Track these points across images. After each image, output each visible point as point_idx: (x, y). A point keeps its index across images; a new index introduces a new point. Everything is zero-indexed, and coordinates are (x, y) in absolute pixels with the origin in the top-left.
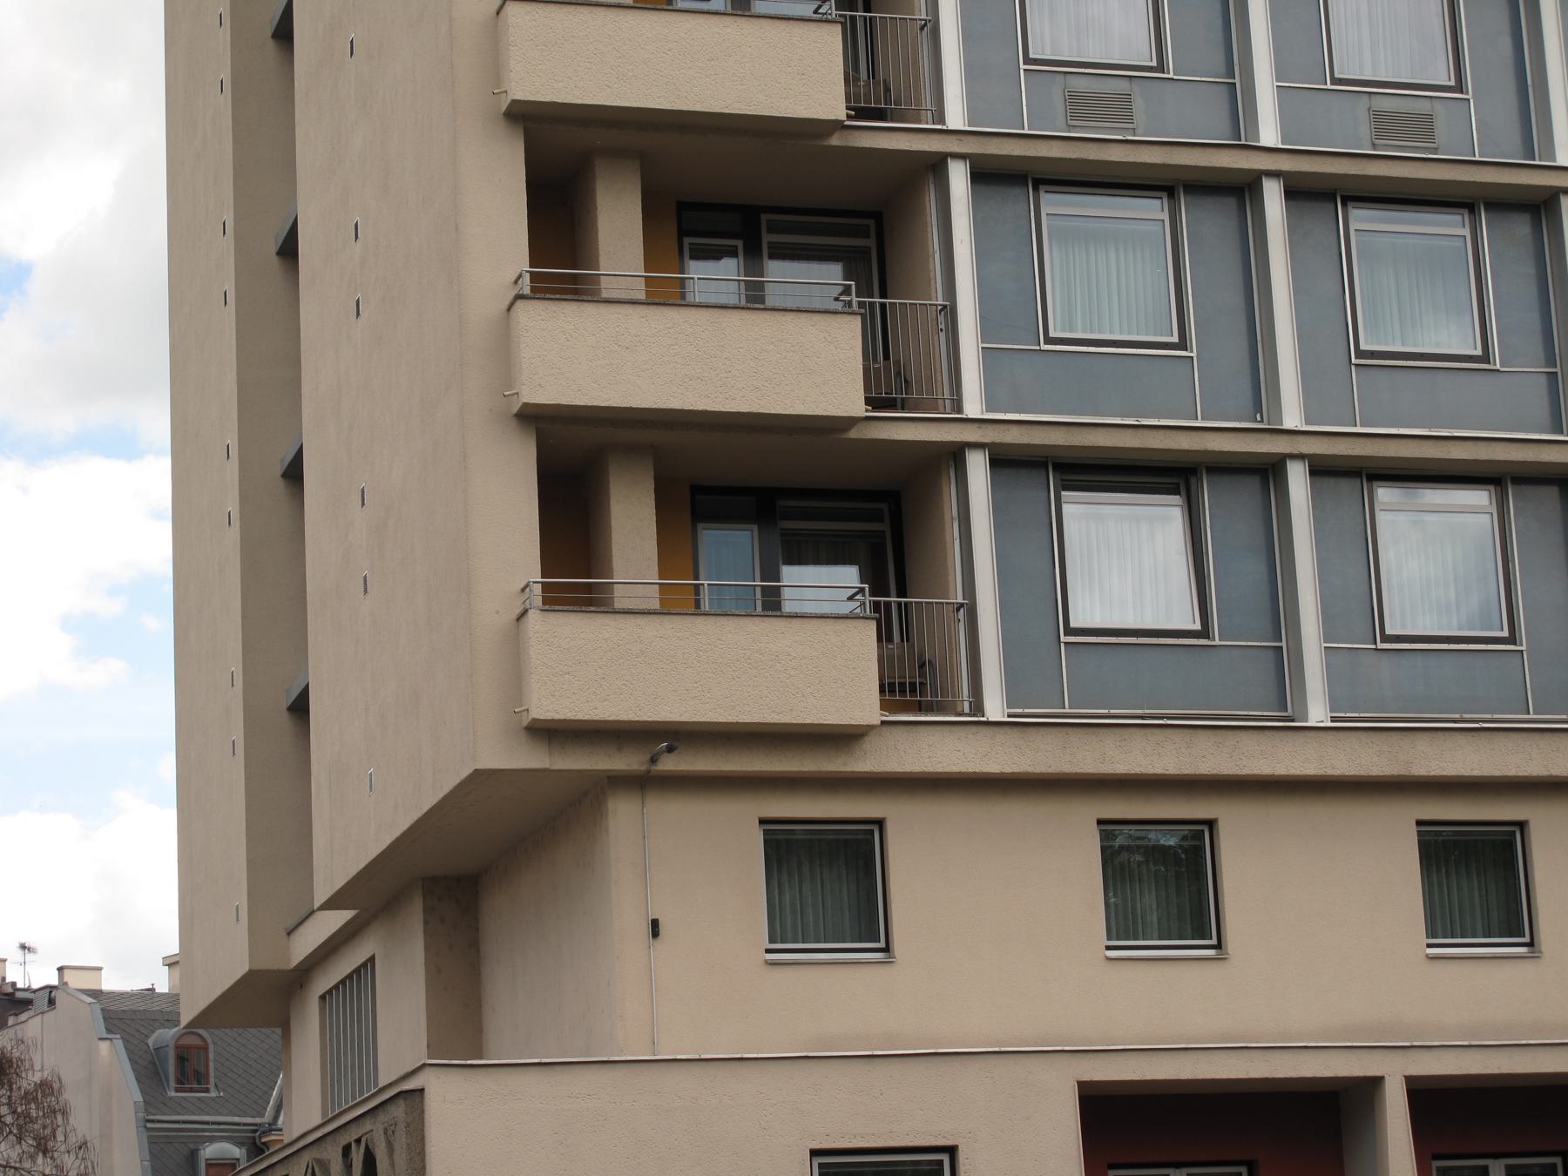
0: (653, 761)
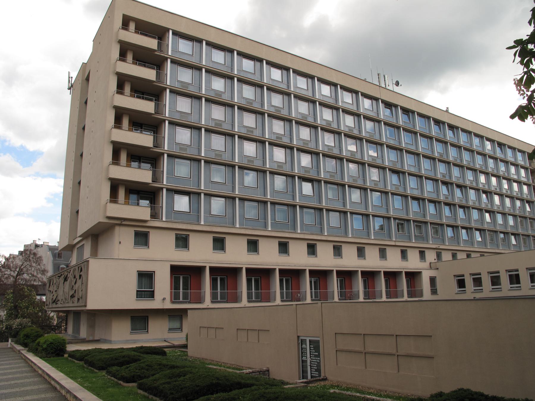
0: (122, 222)
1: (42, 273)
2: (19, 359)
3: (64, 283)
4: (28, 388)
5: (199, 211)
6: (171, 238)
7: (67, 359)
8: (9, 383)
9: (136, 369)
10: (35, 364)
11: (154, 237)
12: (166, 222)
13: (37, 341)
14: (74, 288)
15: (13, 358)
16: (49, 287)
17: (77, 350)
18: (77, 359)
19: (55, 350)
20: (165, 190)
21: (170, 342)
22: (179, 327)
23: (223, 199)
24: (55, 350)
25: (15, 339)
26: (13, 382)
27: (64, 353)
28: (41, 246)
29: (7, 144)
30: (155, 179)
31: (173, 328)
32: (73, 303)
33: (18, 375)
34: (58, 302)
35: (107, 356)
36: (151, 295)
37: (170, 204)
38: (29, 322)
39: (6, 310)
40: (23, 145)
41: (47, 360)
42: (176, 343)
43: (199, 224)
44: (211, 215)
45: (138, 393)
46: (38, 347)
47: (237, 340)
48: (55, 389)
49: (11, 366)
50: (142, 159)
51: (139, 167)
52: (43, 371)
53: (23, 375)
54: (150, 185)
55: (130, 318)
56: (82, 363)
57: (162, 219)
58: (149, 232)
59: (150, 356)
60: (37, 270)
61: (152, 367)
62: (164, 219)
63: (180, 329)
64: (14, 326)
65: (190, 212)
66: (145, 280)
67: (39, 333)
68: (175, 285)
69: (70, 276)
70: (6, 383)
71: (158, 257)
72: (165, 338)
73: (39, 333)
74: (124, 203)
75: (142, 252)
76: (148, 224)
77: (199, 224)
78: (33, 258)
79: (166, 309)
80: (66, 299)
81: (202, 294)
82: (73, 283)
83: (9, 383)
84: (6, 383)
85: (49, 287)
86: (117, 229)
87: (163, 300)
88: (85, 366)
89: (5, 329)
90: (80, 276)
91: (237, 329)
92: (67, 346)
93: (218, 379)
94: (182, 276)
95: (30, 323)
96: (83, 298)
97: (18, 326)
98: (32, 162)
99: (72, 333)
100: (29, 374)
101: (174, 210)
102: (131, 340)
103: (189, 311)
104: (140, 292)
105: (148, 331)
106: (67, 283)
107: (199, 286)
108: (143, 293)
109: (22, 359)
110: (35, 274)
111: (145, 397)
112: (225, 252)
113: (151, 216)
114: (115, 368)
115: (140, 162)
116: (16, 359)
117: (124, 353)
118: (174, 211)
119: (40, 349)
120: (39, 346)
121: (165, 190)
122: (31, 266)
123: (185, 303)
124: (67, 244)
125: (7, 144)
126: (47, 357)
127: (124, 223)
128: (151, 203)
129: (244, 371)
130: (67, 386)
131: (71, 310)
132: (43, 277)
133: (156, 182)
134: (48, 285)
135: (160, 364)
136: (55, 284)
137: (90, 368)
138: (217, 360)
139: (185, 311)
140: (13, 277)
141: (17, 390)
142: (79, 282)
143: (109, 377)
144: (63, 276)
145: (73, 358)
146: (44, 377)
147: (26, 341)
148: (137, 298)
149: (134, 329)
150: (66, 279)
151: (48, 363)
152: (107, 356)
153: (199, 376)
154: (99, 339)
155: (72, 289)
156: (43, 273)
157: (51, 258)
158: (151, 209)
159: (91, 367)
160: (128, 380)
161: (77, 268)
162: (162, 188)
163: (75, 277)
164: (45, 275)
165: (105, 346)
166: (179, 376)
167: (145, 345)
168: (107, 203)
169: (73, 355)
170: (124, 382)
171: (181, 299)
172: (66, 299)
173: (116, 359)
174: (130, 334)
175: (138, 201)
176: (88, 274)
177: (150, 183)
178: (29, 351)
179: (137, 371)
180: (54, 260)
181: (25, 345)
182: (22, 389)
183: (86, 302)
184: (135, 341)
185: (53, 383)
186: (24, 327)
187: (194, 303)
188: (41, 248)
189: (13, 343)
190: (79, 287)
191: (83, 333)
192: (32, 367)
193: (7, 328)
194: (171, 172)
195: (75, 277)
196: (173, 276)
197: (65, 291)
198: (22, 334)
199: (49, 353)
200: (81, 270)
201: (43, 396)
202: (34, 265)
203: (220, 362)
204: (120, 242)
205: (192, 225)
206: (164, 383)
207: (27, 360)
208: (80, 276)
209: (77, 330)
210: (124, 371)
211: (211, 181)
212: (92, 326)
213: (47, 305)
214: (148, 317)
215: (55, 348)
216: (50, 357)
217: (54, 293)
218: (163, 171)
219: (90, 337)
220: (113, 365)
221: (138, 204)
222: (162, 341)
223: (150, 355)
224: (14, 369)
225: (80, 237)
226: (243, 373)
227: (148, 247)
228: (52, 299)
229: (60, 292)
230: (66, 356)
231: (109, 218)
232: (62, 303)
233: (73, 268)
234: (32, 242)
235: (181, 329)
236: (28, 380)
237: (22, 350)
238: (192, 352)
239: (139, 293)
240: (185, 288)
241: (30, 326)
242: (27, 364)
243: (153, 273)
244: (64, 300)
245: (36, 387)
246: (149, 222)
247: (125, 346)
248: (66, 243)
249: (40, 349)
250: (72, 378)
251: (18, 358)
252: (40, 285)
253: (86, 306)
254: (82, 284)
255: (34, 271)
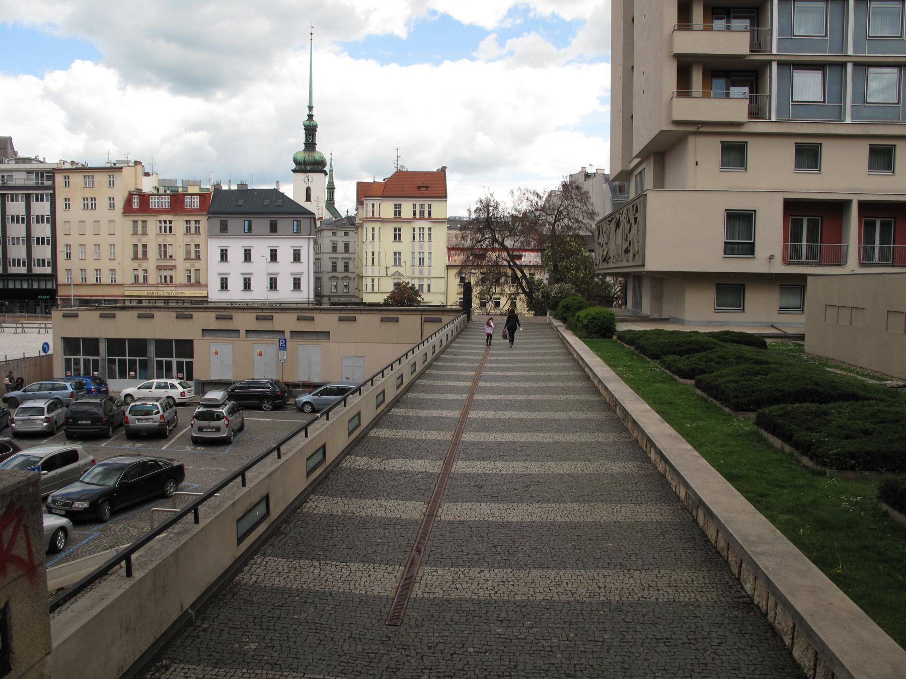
0: (698, 129)
1: (590, 216)
2: (555, 338)
3: (616, 231)
4: (556, 373)
5: (842, 97)
6: (787, 152)
7: (616, 342)
8: (534, 365)
9: (701, 361)
10: (571, 345)
11: (755, 152)
12: (778, 123)
13: (577, 314)
14: (628, 239)
15: (547, 336)
16: (598, 238)
17: (630, 331)
18: (627, 343)
19: (599, 328)
20: (774, 66)
21: (780, 328)
22: (799, 306)
23: (895, 70)
24: (599, 328)
25: (553, 312)
26: (539, 365)
27: (613, 334)
28: (593, 175)
29: (531, 15)
30: (757, 45)
31: (788, 306)
32: (628, 261)
33: (548, 357)
34: (609, 261)
35: (666, 340)
36: (749, 250)
37: (786, 87)
38: (572, 288)
39: (548, 272)
40: (556, 12)
41: (589, 341)
42: (790, 331)
43: (841, 123)
44: (867, 103)
45: (694, 394)
46: (578, 323)
47: (887, 330)
48: (588, 377)
49: (542, 346)
50: (733, 13)
51: (728, 29)
52: (578, 354)
53: (554, 358)
54: (747, 58)
55: (714, 286)
56: (632, 348)
57: (770, 118)
58: (747, 143)
59: (733, 346)
60: (582, 212)
61: (726, 359)
62: (774, 118)
63: (800, 308)
64: (553, 294)
65: (824, 102)
66: (739, 225)
67: (582, 304)
68: (792, 233)
69: (623, 220)
70: (531, 365)
71: (763, 185)
72: (772, 323)
73: (582, 304)
74: (701, 96)
75: (734, 178)
76: (745, 129)
77: (841, 123)
78: (576, 195)
79: (777, 274)
80: (618, 255)
81: (844, 250)
82: (627, 231)
83: (534, 365)
84: (531, 365)
85: (598, 238)
86: (691, 140)
87: (770, 258)
88: (636, 352)
89: (542, 298)
90: (636, 219)
91: (888, 311)
92: (617, 324)
93: (817, 384)
94: (807, 218)
95: (574, 290)
96: (640, 254)
97: (557, 293)
98: (570, 39)
99: (632, 308)
100: (562, 358)
101: (794, 100)
102: (716, 322)
103: (809, 278)
104: (731, 246)
105: (743, 309)
106: (620, 231)
107: (839, 235)
108: (737, 246)
109: (559, 338)
110: (580, 218)
111: (702, 398)
112: (893, 172)
113: (749, 114)
114: (671, 357)
115: (730, 18)
116: (551, 338)
117: (693, 338)
118: (792, 101)
119: (580, 325)
120: (579, 321)
121: (774, 66)
122: (574, 207)
123: (811, 264)
124: (620, 170)
125: (531, 15)
126: (588, 337)
127: (702, 129)
128: (751, 91)
129: (889, 382)
130: (599, 374)
131: (631, 272)
132: (591, 222)
133: (760, 52)
134: (596, 234)
135: (740, 356)
136: (605, 232)
137: (641, 355)
138: (851, 362)
139: (804, 277)
140: (550, 223)
141: (542, 374)
142: (634, 228)
143: (663, 369)
144: (614, 221)
145: (622, 341)
146: (579, 363)
147: (565, 315)
148: (725, 254)
149: (721, 304)
150: (618, 225)
151: (587, 345)
152: (666, 340)
153: (788, 377)
154: (667, 317)
155: (626, 240)
156: (592, 217)
157: (609, 194)
158: (751, 102)
159: (643, 354)
160: (685, 375)
161: (631, 207)
162: (769, 63)
163: (629, 222)
164: (594, 220)
165: (669, 328)
166: (756, 374)
167: (732, 329)
168: (672, 98)
169: (622, 337)
170: (679, 376)
171: (804, 259)
172: (618, 255)
173: (678, 345)
174: (715, 312)
175: (728, 89)
176: (645, 217)
177: (746, 56)
178: (568, 328)
179: (700, 363)
180: (613, 197)
181: (564, 320)
182: (548, 373)
183: (644, 260)
184: (723, 323)
185: (587, 369)
186: (566, 296)
187: (826, 265)
188: (594, 179)
189: (551, 318)
190: (634, 236)
191: (646, 309)
192: (568, 349)
193: (543, 296)
194: (786, 29)
195: (629, 222)
196: (791, 217)
197: (617, 243)
198: (560, 304)
199: (591, 332)
200: (637, 211)
201: (570, 384)
202: (578, 204)
203: (854, 366)
204: (697, 163)
205: (827, 125)
206: (729, 382)
207: (563, 340)
208: (636, 219)
209: (638, 304)
210: (683, 363)
211: (869, 37)
212: (658, 298)
213: (596, 265)
214: (744, 286)
215: (599, 326)
216: (593, 338)
217: (604, 245)
218: (771, 30)
219: (655, 314)
220: (672, 353)
221: (727, 95)
222: (768, 326)
223: (736, 345)
224: (545, 349)
225: (636, 157)
226: (885, 385)
227: (746, 169)
228: (603, 256)
229: (612, 245)
230: (615, 337)
231: (677, 123)
232: (614, 261)
233: (626, 207)
234: (581, 170)
235: (801, 308)
236: (558, 364)
237: (561, 326)
238: (810, 346)
239: (728, 246)
240: (812, 238)
241: (574, 295)
242: (563, 345)
243: (754, 213)
244: (617, 257)
245: (565, 373)
246: (745, 125)
247: (702, 330)
248: (619, 170)
249: (580, 325)
250: (610, 366)
251: (554, 336)
252: (588, 236)
253: (644, 266)
254: (638, 231)
255: (578, 214)
